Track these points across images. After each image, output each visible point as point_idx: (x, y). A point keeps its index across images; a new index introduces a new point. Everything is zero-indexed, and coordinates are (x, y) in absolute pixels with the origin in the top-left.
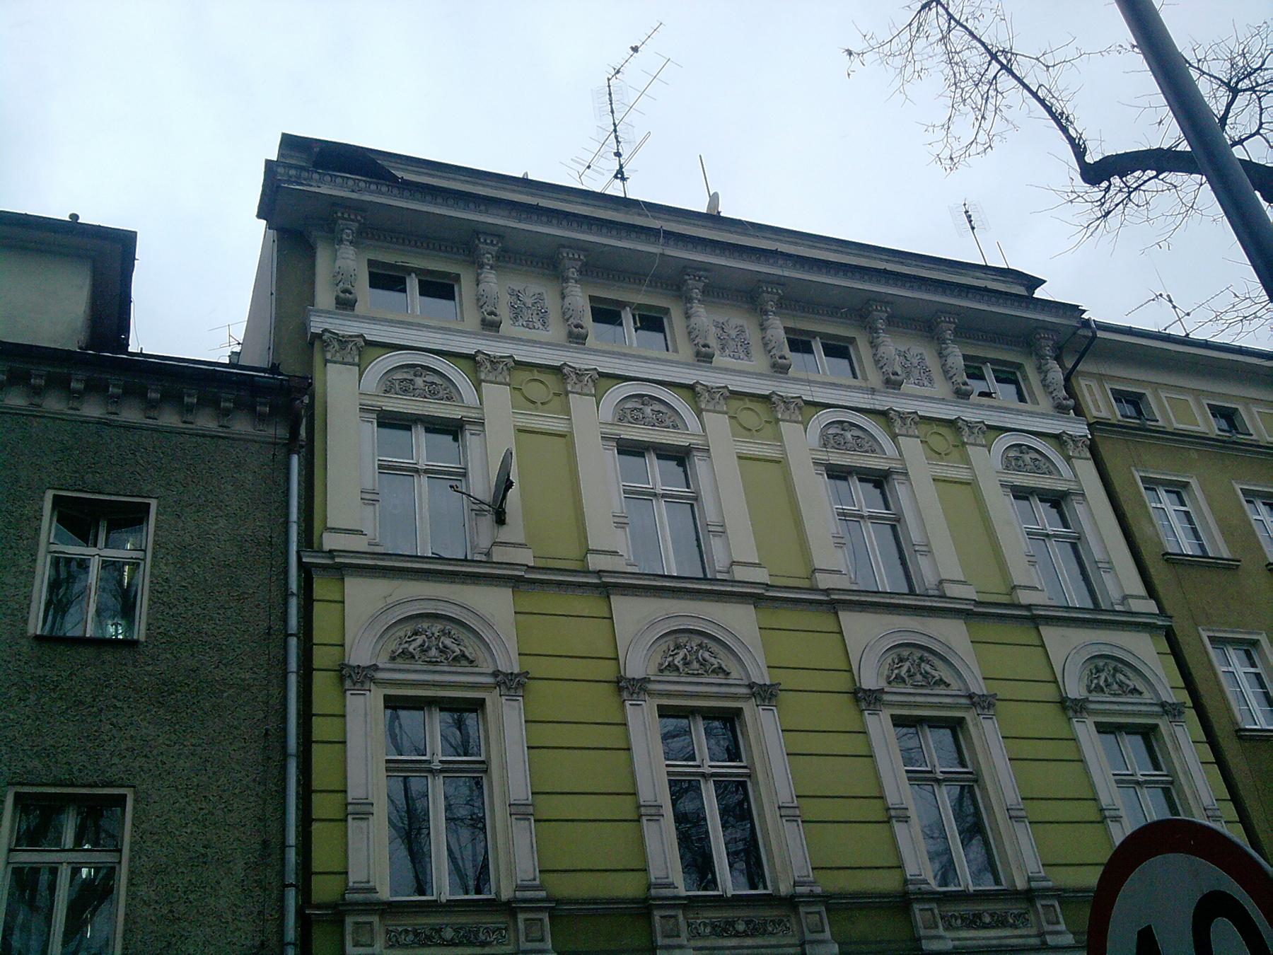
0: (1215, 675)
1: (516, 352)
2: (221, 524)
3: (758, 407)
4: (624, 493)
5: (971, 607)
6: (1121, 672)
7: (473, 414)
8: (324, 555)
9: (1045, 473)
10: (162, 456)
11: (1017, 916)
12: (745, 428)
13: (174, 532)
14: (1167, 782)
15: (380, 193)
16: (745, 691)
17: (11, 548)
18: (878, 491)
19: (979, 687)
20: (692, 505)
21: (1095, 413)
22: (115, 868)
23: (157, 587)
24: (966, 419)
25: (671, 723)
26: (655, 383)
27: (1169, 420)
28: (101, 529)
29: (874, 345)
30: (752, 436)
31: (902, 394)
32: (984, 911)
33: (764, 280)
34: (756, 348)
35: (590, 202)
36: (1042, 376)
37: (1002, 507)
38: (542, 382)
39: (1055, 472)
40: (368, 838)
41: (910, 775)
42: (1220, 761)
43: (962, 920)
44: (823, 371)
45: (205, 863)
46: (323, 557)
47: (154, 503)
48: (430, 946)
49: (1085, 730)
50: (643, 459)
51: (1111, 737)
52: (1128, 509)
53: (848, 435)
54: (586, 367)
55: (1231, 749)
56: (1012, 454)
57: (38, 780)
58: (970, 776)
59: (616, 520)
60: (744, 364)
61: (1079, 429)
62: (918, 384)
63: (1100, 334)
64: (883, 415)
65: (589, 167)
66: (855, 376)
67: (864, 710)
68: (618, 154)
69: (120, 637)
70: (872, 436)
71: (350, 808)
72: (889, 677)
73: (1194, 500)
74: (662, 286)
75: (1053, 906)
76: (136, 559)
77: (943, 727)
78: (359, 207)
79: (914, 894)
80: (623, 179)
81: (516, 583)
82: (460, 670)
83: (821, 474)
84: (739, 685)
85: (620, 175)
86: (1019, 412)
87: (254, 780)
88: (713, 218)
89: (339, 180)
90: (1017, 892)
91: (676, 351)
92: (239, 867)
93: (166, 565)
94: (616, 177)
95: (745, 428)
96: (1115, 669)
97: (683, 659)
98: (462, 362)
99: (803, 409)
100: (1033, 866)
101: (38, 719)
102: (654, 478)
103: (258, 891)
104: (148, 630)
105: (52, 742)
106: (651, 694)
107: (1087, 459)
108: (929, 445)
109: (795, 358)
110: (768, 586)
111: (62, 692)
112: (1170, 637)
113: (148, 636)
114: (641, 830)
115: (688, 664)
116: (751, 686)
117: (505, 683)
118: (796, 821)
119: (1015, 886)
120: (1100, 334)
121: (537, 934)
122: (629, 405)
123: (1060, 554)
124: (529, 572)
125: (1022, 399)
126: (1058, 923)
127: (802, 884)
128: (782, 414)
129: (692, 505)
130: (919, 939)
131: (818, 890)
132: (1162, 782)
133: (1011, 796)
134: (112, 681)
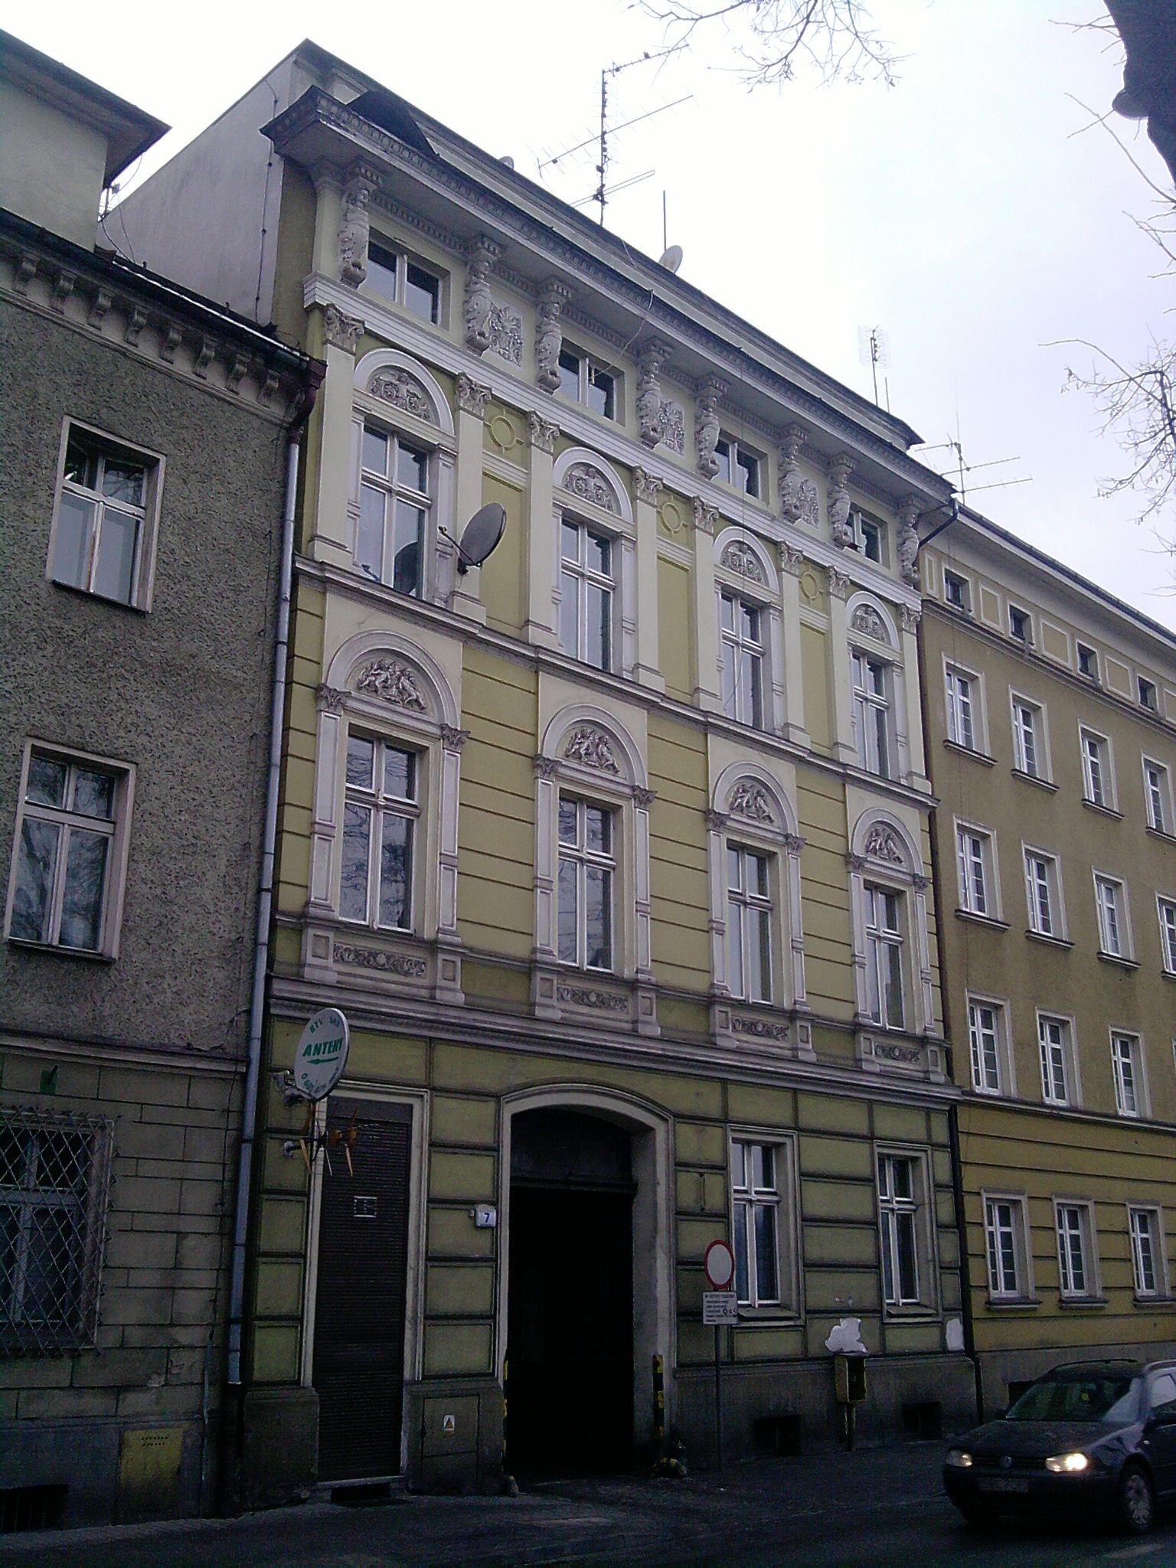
0: (954, 858)
1: (498, 386)
2: (223, 503)
3: (513, 420)
4: (363, 479)
5: (805, 756)
6: (892, 839)
7: (447, 443)
8: (314, 564)
9: (754, 579)
10: (172, 407)
11: (783, 1030)
12: (495, 441)
13: (181, 499)
14: (896, 941)
15: (409, 162)
16: (436, 731)
17: (31, 474)
18: (417, 466)
19: (793, 830)
20: (421, 512)
21: (929, 591)
22: (107, 839)
23: (164, 558)
24: (646, 471)
25: (568, 807)
26: (757, 536)
27: (978, 613)
28: (99, 469)
29: (468, 290)
30: (500, 453)
31: (794, 529)
32: (759, 1021)
33: (715, 373)
34: (688, 441)
35: (576, 224)
36: (900, 541)
37: (709, 600)
38: (675, 510)
39: (763, 580)
40: (329, 859)
41: (349, 793)
42: (939, 934)
43: (573, 996)
44: (734, 482)
45: (194, 853)
46: (314, 568)
47: (163, 459)
48: (366, 967)
49: (717, 843)
50: (575, 532)
51: (735, 853)
52: (930, 690)
53: (592, 482)
54: (655, 475)
55: (949, 921)
56: (385, 378)
57: (54, 738)
58: (767, 904)
59: (351, 509)
60: (510, 367)
61: (914, 604)
62: (669, 446)
63: (960, 517)
64: (453, 381)
65: (555, 161)
66: (434, 319)
67: (321, 711)
68: (600, 169)
69: (92, 591)
70: (613, 489)
71: (317, 827)
72: (732, 804)
73: (1039, 725)
74: (386, 205)
75: (807, 1028)
76: (137, 516)
77: (754, 856)
78: (384, 170)
79: (643, 983)
80: (603, 202)
81: (467, 637)
82: (411, 713)
83: (358, 424)
84: (623, 784)
85: (600, 196)
86: (601, 427)
87: (239, 782)
88: (663, 272)
89: (376, 134)
90: (784, 1011)
91: (622, 422)
92: (222, 864)
93: (172, 534)
94: (595, 197)
95: (495, 441)
96: (889, 837)
97: (383, 681)
98: (443, 378)
99: (558, 439)
100: (801, 995)
101: (54, 673)
102: (583, 557)
103: (236, 889)
104: (155, 602)
105: (67, 700)
106: (349, 711)
107: (913, 634)
108: (491, 433)
109: (369, 267)
110: (664, 697)
111: (77, 649)
112: (932, 818)
113: (154, 609)
114: (310, 851)
115: (589, 754)
116: (634, 788)
117: (326, 697)
118: (646, 917)
119: (623, 973)
120: (960, 517)
121: (450, 975)
122: (384, 378)
123: (586, 597)
124: (484, 633)
125: (608, 414)
126: (808, 1042)
127: (643, 972)
128: (465, 402)
129: (421, 512)
130: (534, 1004)
131: (653, 979)
132: (890, 940)
133: (642, 893)
134: (121, 649)
